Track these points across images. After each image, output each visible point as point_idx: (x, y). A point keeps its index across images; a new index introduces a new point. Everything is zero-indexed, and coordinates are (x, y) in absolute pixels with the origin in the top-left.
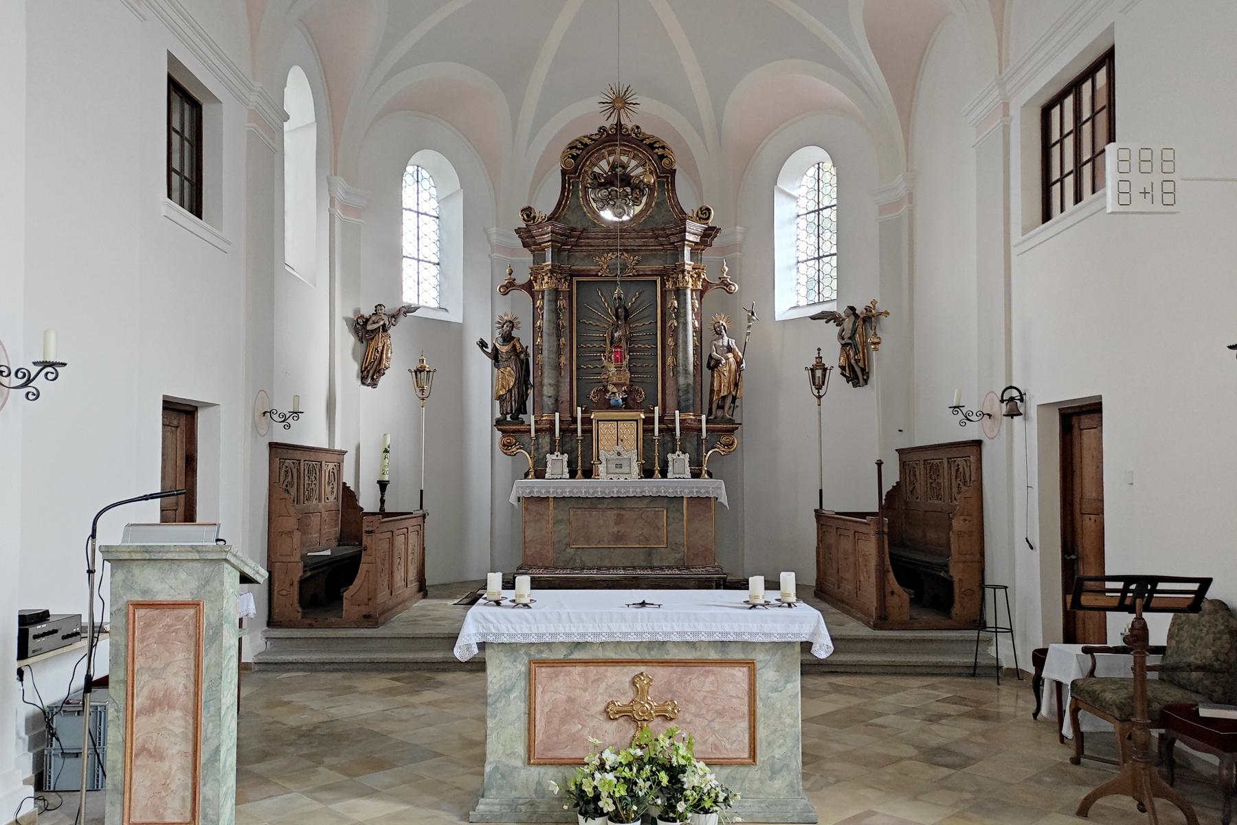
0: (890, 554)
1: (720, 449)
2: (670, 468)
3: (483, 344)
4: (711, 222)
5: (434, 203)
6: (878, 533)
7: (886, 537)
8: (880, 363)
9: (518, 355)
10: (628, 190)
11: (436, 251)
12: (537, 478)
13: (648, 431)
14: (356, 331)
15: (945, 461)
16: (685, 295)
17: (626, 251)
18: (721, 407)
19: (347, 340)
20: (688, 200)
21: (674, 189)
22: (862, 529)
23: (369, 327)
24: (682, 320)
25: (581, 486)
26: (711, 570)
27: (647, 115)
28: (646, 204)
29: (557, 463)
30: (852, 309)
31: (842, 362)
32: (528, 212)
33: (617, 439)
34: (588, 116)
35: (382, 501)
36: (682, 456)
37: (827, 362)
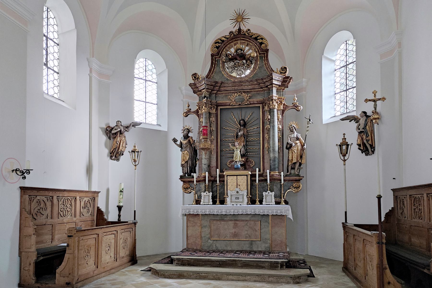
0: (386, 249)
1: (293, 190)
2: (264, 200)
3: (175, 141)
4: (287, 74)
5: (155, 76)
6: (378, 243)
7: (384, 246)
8: (382, 134)
9: (191, 145)
10: (244, 61)
11: (152, 98)
12: (197, 204)
13: (253, 181)
14: (107, 134)
15: (425, 195)
16: (273, 112)
17: (244, 92)
18: (293, 168)
19: (100, 140)
20: (274, 62)
21: (267, 60)
22: (368, 238)
23: (113, 132)
24: (272, 125)
25: (218, 209)
26: (281, 255)
27: (253, 25)
28: (254, 68)
29: (207, 197)
30: (365, 113)
31: (359, 142)
32: (195, 76)
33: (237, 185)
34: (226, 27)
35: (119, 216)
36: (270, 193)
37: (349, 141)
